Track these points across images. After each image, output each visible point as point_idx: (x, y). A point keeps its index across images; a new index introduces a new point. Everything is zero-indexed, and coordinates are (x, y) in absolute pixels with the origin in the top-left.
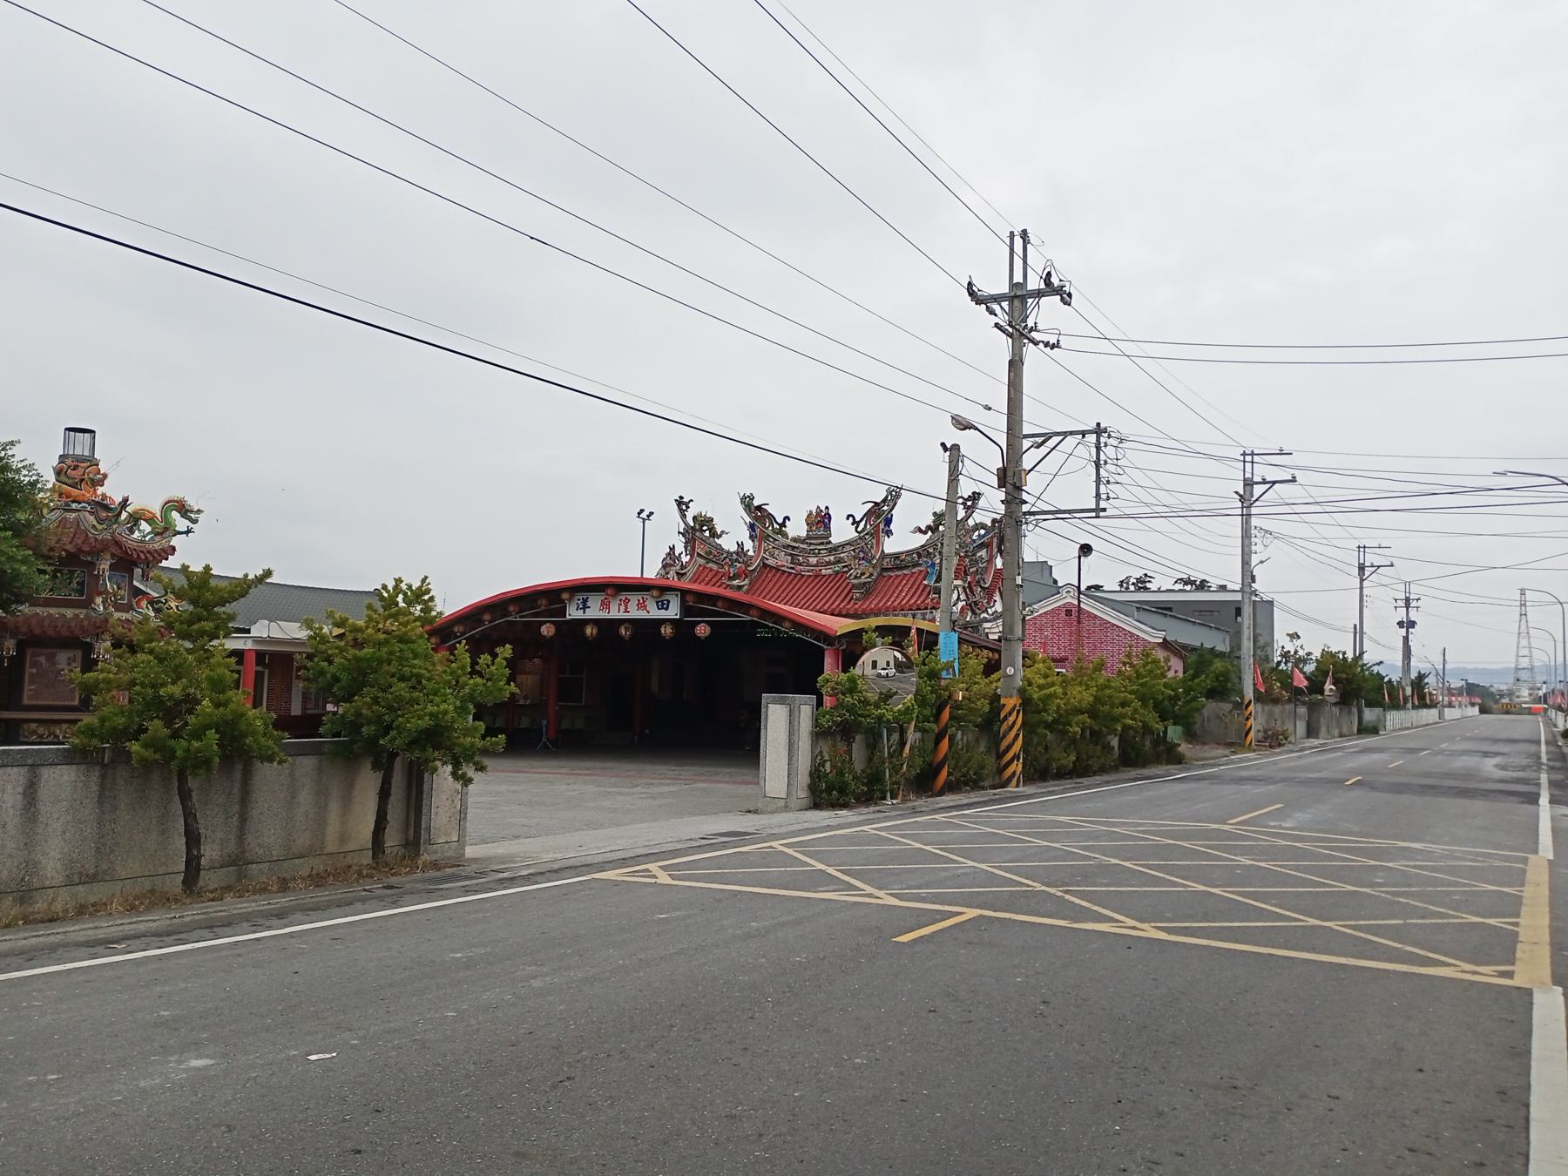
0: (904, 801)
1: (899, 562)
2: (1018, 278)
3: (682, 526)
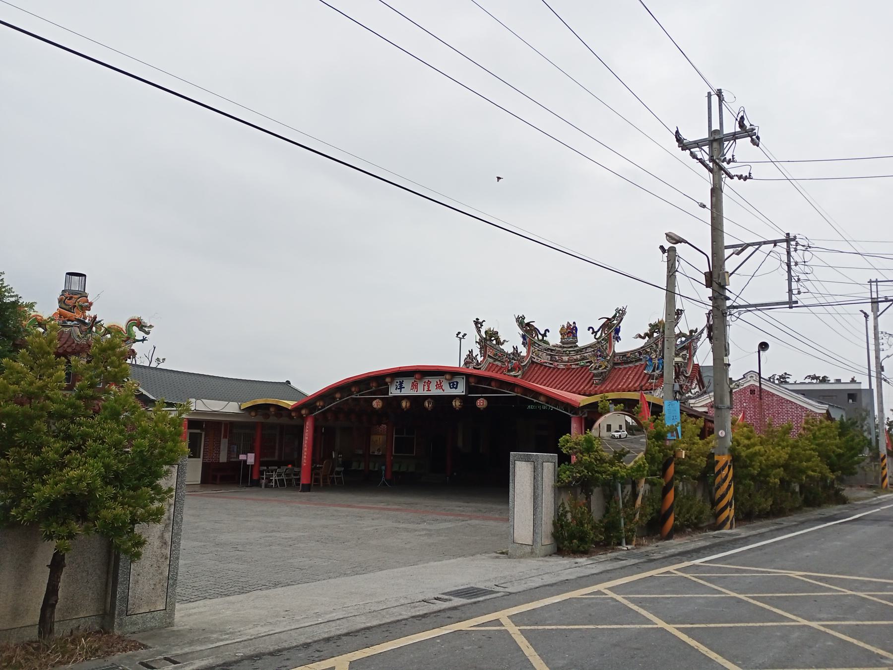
0: (638, 545)
1: (626, 358)
2: (716, 126)
3: (478, 337)
